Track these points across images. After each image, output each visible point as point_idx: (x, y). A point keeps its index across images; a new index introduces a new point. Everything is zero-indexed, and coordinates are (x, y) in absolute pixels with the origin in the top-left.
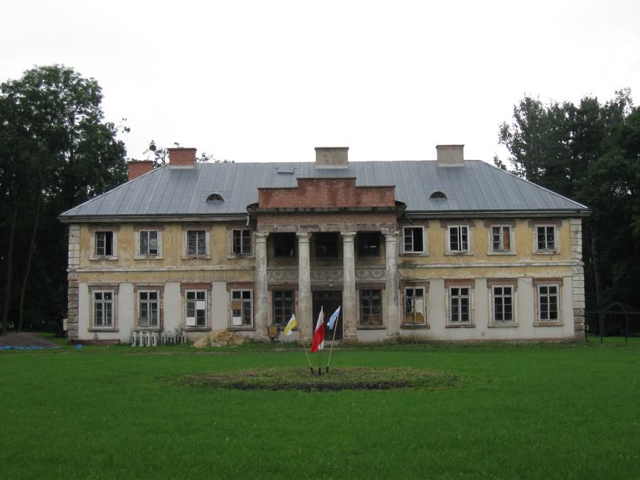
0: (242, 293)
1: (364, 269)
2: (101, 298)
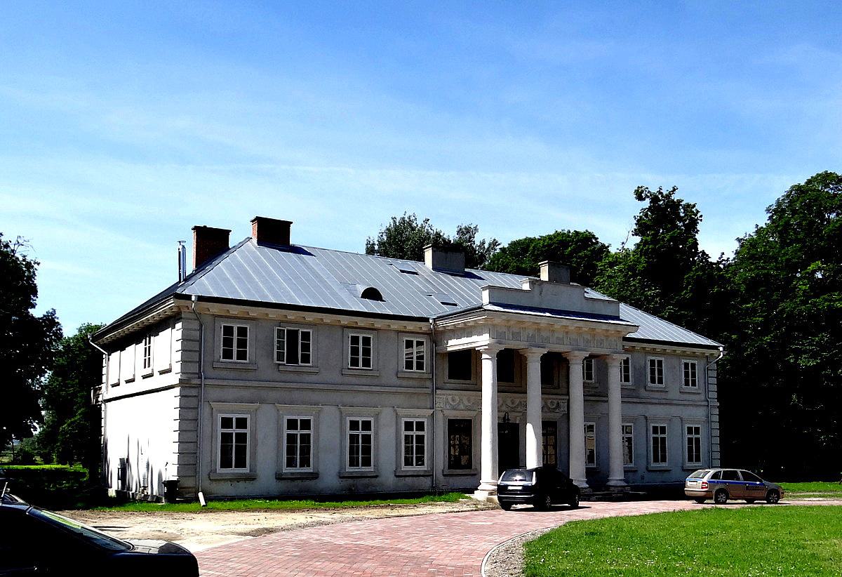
0: (360, 429)
1: (262, 401)
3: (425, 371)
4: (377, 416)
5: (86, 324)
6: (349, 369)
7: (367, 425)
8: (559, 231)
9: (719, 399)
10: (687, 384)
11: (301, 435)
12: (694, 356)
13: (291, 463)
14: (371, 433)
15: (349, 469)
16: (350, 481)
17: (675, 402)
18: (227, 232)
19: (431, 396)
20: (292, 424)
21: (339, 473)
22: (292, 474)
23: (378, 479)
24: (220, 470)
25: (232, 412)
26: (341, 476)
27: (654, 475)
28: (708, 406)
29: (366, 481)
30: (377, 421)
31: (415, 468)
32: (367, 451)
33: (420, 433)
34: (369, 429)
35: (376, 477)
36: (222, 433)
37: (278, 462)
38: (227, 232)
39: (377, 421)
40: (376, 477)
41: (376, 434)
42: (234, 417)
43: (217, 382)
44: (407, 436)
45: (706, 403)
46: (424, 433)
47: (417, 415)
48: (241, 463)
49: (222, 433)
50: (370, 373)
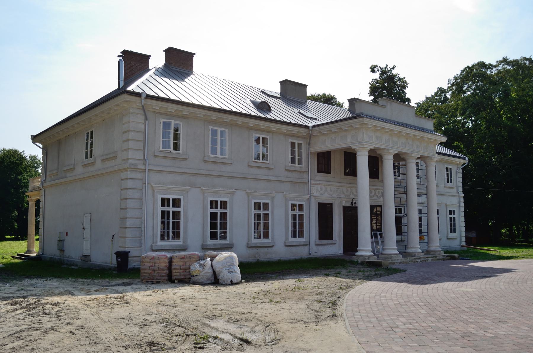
2: (174, 206)
3: (303, 166)
4: (273, 198)
5: (317, 94)
6: (253, 162)
7: (266, 206)
8: (484, 62)
9: (464, 192)
10: (448, 182)
11: (221, 213)
12: (451, 163)
13: (213, 236)
14: (227, 211)
15: (255, 241)
16: (255, 250)
17: (443, 193)
18: (148, 57)
19: (308, 185)
20: (214, 204)
21: (202, 245)
22: (215, 245)
23: (273, 248)
24: (160, 243)
25: (170, 194)
26: (249, 246)
27: (294, 249)
28: (459, 196)
29: (266, 250)
30: (273, 202)
31: (298, 240)
32: (224, 226)
33: (266, 212)
34: (179, 206)
35: (272, 246)
36: (211, 213)
37: (287, 238)
38: (148, 57)
39: (273, 202)
40: (272, 246)
41: (272, 213)
42: (171, 197)
43: (157, 168)
44: (163, 212)
45: (457, 195)
46: (180, 209)
47: (299, 199)
48: (176, 235)
49: (211, 213)
50: (268, 166)
